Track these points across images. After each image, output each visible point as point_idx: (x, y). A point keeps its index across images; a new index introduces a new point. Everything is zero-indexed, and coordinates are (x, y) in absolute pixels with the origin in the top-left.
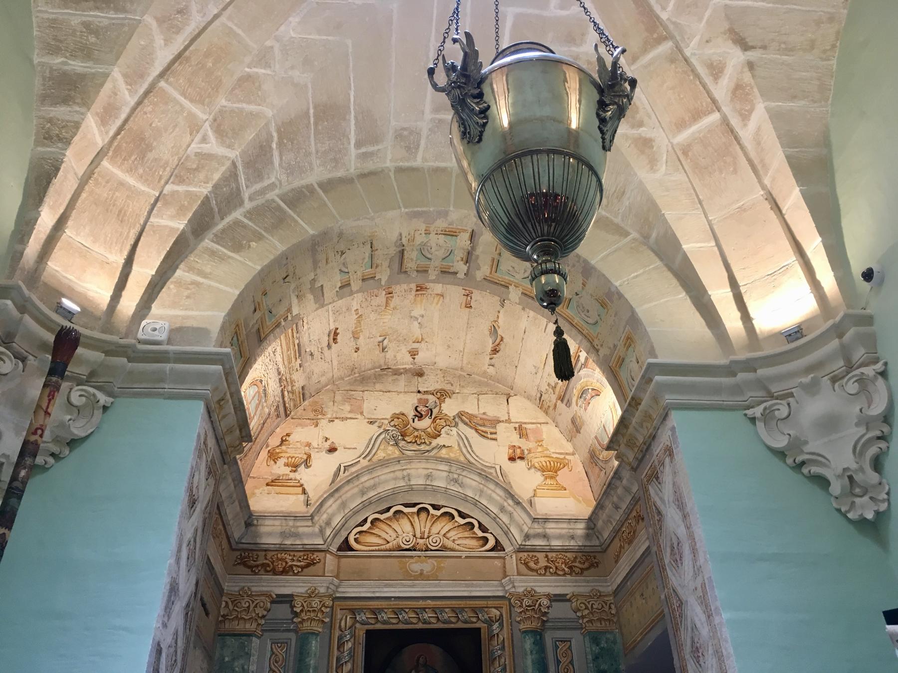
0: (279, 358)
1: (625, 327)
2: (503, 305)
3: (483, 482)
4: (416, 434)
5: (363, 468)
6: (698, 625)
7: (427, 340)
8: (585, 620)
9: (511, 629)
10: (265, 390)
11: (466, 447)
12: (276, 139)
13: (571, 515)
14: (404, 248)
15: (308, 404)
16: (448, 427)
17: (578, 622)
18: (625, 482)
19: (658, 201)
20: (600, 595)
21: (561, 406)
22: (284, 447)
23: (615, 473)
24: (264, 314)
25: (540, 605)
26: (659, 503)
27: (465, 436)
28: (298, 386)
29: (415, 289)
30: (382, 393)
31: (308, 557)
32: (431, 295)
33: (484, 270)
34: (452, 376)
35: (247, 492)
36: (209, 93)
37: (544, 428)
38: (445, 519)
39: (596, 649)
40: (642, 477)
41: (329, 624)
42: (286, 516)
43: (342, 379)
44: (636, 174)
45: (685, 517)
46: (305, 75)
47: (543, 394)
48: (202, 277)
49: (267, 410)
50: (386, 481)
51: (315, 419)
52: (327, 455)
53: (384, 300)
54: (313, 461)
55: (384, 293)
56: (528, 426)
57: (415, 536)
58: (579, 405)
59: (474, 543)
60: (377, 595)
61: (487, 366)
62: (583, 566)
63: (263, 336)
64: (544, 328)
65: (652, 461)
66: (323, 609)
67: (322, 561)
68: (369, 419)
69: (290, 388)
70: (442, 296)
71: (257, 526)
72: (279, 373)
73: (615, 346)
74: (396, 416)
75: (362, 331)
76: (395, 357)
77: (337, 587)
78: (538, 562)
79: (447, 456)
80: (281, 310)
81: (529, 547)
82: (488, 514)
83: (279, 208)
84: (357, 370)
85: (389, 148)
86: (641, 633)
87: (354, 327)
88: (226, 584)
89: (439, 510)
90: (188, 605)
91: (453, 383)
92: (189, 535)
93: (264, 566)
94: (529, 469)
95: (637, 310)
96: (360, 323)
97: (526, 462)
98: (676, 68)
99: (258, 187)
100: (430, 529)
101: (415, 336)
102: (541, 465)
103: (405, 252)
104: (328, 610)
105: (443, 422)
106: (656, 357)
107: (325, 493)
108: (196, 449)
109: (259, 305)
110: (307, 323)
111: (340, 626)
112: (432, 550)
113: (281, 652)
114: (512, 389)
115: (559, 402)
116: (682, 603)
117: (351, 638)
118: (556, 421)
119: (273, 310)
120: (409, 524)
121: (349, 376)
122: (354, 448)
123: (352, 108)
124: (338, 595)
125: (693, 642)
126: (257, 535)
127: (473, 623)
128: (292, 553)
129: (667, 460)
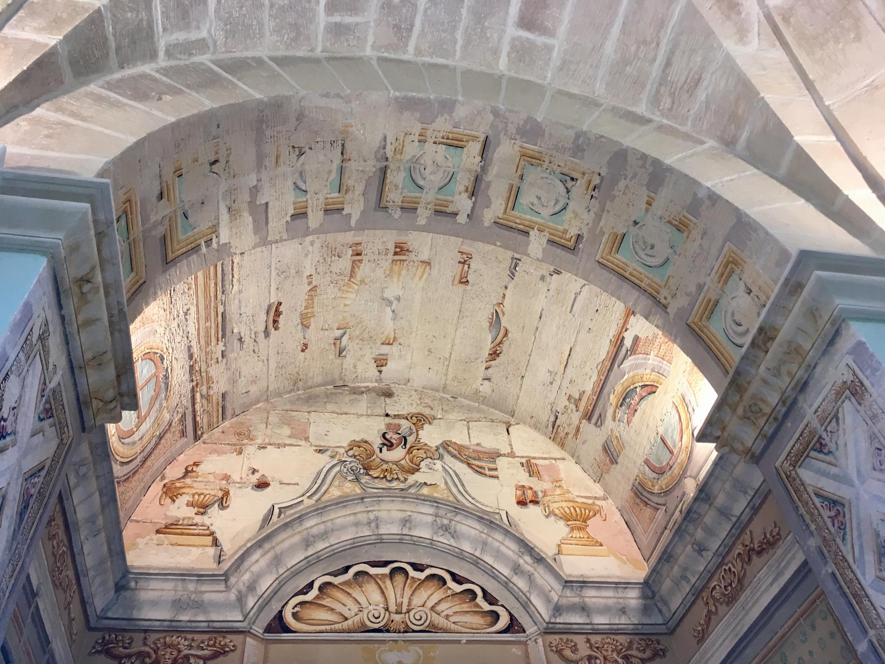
0: (192, 329)
3: (485, 531)
4: (385, 467)
7: (401, 340)
10: (166, 377)
11: (456, 486)
13: (618, 577)
14: (387, 163)
15: (229, 425)
16: (429, 460)
19: (754, 81)
22: (188, 481)
27: (455, 472)
29: (392, 250)
30: (336, 415)
31: (215, 642)
32: (414, 262)
33: (495, 209)
34: (431, 399)
35: (125, 541)
37: (561, 465)
38: (432, 585)
40: (778, 464)
42: (183, 575)
44: (720, 46)
47: (559, 415)
49: (167, 416)
50: (343, 528)
53: (349, 265)
55: (350, 252)
56: (540, 462)
57: (387, 609)
58: (617, 419)
59: (477, 620)
61: (480, 381)
63: (171, 256)
68: (316, 446)
69: (204, 392)
70: (429, 264)
72: (191, 356)
73: (700, 287)
74: (354, 444)
76: (355, 367)
78: (577, 650)
81: (561, 626)
82: (495, 577)
83: (211, 70)
84: (301, 383)
87: (304, 305)
89: (422, 571)
94: (547, 517)
100: (410, 599)
101: (386, 334)
102: (562, 511)
103: (389, 171)
105: (422, 453)
107: (249, 540)
110: (239, 281)
112: (414, 631)
114: (513, 416)
118: (576, 455)
119: (189, 213)
121: (290, 392)
122: (294, 484)
126: (133, 604)
128: (189, 636)
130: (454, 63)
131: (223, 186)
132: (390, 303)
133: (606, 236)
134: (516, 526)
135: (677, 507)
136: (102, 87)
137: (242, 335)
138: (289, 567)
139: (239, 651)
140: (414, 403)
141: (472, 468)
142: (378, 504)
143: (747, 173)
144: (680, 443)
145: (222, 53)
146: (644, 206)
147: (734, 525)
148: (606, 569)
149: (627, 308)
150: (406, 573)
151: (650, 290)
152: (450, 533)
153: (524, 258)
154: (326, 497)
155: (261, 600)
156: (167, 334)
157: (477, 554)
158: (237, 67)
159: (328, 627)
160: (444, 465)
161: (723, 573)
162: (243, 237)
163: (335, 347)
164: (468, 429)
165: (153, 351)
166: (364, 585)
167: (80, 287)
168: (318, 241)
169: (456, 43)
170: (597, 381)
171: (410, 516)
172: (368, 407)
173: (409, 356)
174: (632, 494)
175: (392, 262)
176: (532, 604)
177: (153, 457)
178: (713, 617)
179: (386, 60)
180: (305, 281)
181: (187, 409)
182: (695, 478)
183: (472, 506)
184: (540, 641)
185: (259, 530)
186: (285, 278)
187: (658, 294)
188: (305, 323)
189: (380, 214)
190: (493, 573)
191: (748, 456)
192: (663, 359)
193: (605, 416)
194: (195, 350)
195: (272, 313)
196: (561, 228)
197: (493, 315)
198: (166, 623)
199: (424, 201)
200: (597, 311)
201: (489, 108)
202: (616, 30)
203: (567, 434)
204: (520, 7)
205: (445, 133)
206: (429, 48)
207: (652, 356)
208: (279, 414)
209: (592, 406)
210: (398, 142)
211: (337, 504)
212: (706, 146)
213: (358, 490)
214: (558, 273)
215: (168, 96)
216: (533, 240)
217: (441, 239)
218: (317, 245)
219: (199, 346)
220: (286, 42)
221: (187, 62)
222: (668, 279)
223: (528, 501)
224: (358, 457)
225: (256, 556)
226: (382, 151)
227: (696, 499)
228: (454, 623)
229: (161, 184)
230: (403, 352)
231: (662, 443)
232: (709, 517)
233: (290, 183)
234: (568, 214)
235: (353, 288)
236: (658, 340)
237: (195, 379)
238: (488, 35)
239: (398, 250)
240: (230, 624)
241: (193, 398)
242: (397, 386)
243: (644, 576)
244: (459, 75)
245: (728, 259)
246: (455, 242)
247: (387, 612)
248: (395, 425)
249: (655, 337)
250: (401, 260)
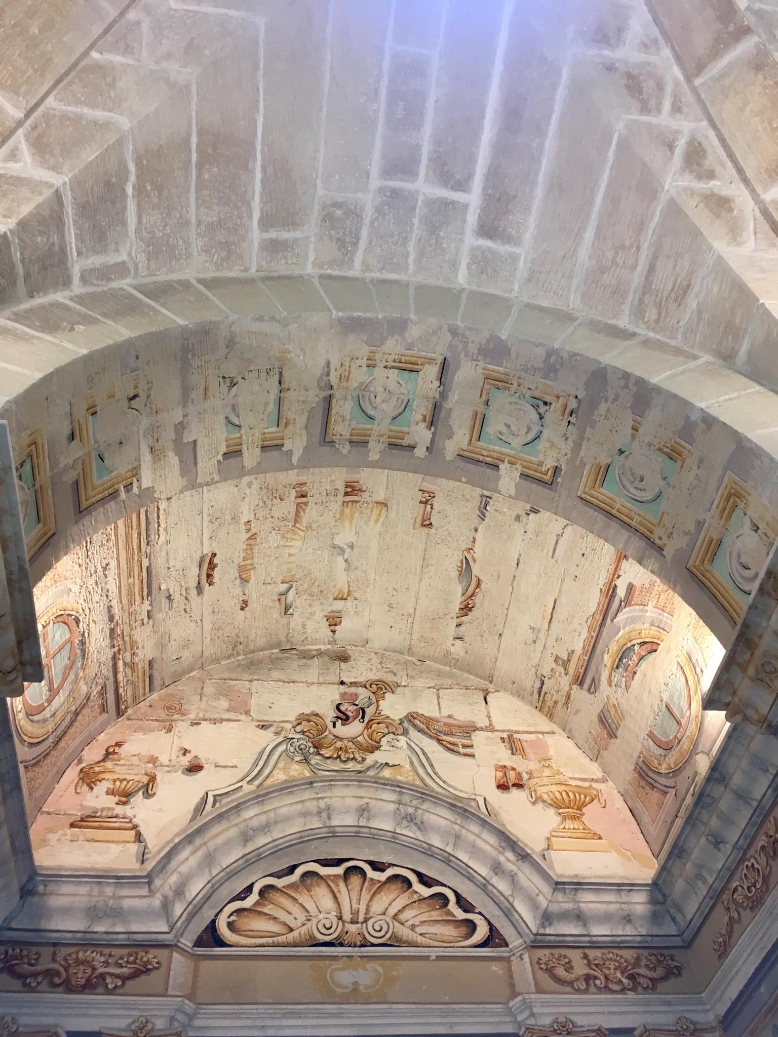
0: (112, 586)
3: (459, 822)
4: (339, 744)
7: (356, 595)
10: (83, 643)
12: (132, 178)
13: (621, 877)
15: (157, 698)
16: (392, 736)
22: (109, 764)
24: (89, 453)
27: (422, 749)
28: (146, 652)
30: (281, 683)
31: (136, 958)
32: (367, 503)
34: (394, 663)
36: (29, 77)
37: (549, 739)
38: (395, 888)
42: (99, 877)
43: (216, 660)
44: (710, 248)
46: (189, 70)
47: (546, 680)
49: (84, 689)
50: (287, 819)
51: (168, 721)
52: (184, 776)
54: (160, 786)
55: (293, 493)
57: (340, 918)
58: (613, 684)
59: (449, 932)
61: (450, 641)
63: (84, 504)
64: (552, 550)
68: (258, 721)
70: (385, 505)
72: (111, 618)
73: (700, 524)
74: (303, 718)
76: (304, 626)
77: (191, 1017)
78: (572, 968)
80: (120, 465)
81: (552, 938)
82: (470, 879)
83: (130, 296)
84: (241, 647)
85: (313, 239)
87: (242, 556)
89: (383, 870)
91: (395, 671)
93: (49, 974)
94: (534, 803)
97: (527, 791)
98: (765, 78)
99: (97, 261)
100: (368, 905)
101: (339, 586)
102: (552, 796)
103: (334, 401)
105: (382, 728)
107: (178, 834)
110: (166, 530)
112: (373, 945)
114: (491, 682)
121: (229, 657)
122: (232, 767)
123: (259, 147)
128: (106, 951)
130: (406, 279)
131: (145, 422)
132: (343, 551)
133: (588, 467)
134: (495, 816)
135: (688, 790)
136: (9, 319)
137: (171, 592)
138: (224, 866)
139: (163, 970)
140: (374, 668)
141: (443, 744)
142: (330, 789)
143: (748, 391)
144: (688, 712)
145: (144, 277)
146: (629, 431)
147: (755, 811)
148: (606, 867)
149: (617, 551)
150: (363, 872)
151: (642, 529)
152: (416, 824)
153: (495, 496)
154: (269, 782)
155: (191, 907)
156: (83, 592)
157: (449, 849)
158: (159, 292)
159: (270, 940)
160: (409, 741)
161: (745, 871)
162: (168, 480)
163: (280, 604)
164: (438, 698)
165: (67, 612)
166: (313, 889)
168: (257, 482)
169: (408, 256)
170: (587, 638)
171: (367, 804)
172: (319, 674)
173: (366, 614)
174: (636, 775)
175: (343, 504)
176: (517, 912)
177: (67, 737)
178: (736, 926)
179: (330, 277)
180: (243, 527)
181: (108, 680)
182: (708, 754)
183: (443, 792)
184: (526, 957)
185: (190, 822)
186: (220, 525)
187: (652, 533)
188: (243, 576)
189: (326, 450)
190: (468, 872)
191: (765, 725)
192: (662, 610)
193: (599, 681)
194: (117, 611)
196: (534, 459)
197: (462, 563)
198: (79, 935)
199: (376, 434)
200: (583, 555)
201: (446, 327)
202: (589, 234)
203: (556, 702)
204: (479, 214)
205: (396, 357)
206: (378, 263)
207: (650, 608)
208: (216, 683)
209: (583, 668)
210: (343, 367)
211: (281, 790)
212: (700, 362)
213: (307, 774)
214: (536, 512)
215: (81, 326)
216: (503, 475)
217: (398, 476)
218: (256, 485)
219: (120, 606)
220: (216, 262)
221: (105, 289)
222: (662, 517)
223: (510, 784)
224: (307, 733)
226: (325, 378)
227: (709, 779)
228: (421, 934)
229: (72, 423)
230: (360, 609)
231: (668, 712)
232: (726, 802)
233: (221, 418)
234: (542, 445)
235: (299, 535)
236: (656, 588)
237: (116, 645)
238: (445, 246)
239: (349, 490)
240: (153, 936)
241: (115, 666)
242: (354, 648)
243: (652, 876)
244: (412, 291)
245: (730, 491)
246: (415, 479)
247: (341, 922)
248: (351, 694)
249: (653, 584)
250: (353, 502)
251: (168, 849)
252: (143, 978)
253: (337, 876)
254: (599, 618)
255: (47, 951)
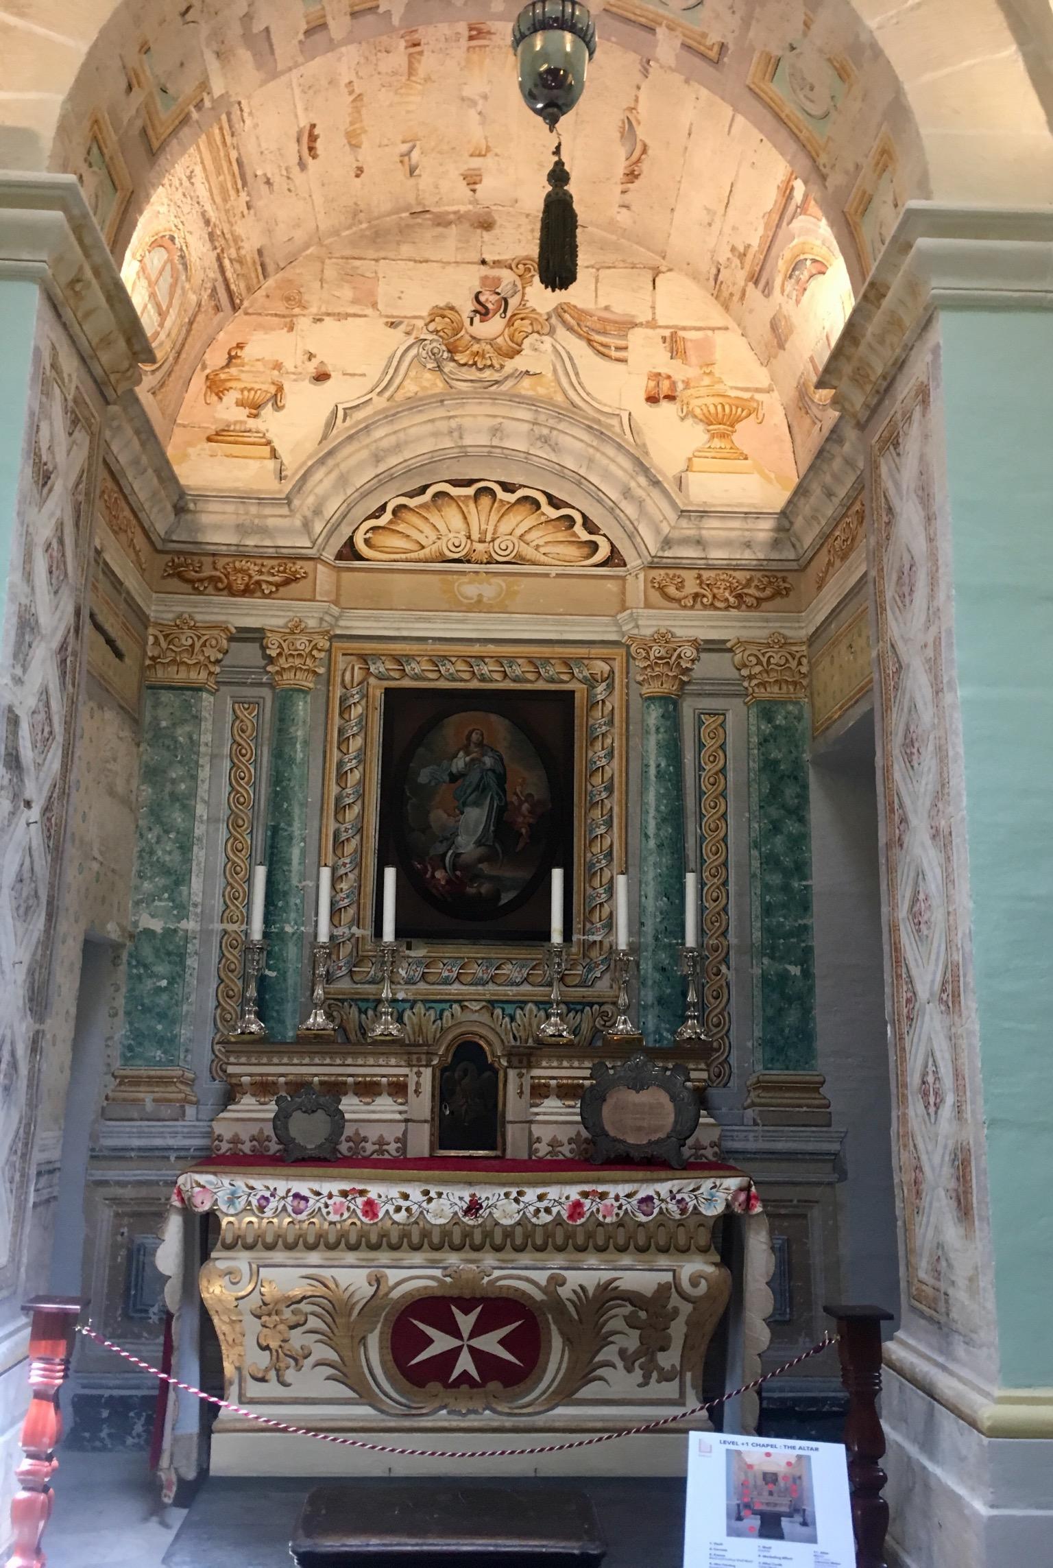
0: (202, 191)
1: (880, 125)
2: (647, 71)
3: (595, 444)
4: (476, 348)
5: (376, 413)
6: (920, 705)
7: (497, 150)
8: (754, 682)
9: (627, 694)
10: (182, 257)
13: (749, 505)
16: (536, 335)
17: (741, 685)
18: (847, 447)
20: (785, 643)
21: (753, 293)
22: (233, 371)
23: (833, 431)
24: (151, 95)
25: (679, 657)
26: (892, 492)
27: (568, 353)
28: (248, 250)
29: (466, 34)
32: (499, 47)
37: (719, 337)
38: (525, 509)
39: (766, 728)
41: (325, 677)
42: (243, 498)
43: (336, 233)
45: (929, 519)
48: (12, 13)
49: (193, 298)
50: (418, 439)
55: (402, 44)
59: (572, 552)
60: (405, 633)
62: (761, 595)
63: (156, 144)
65: (892, 413)
66: (315, 652)
67: (311, 576)
69: (234, 255)
71: (195, 512)
74: (438, 313)
75: (365, 132)
76: (437, 187)
77: (337, 619)
78: (683, 587)
79: (530, 393)
80: (185, 87)
81: (669, 561)
82: (599, 501)
86: (841, 708)
88: (153, 608)
89: (513, 492)
90: (63, 647)
92: (45, 532)
95: (907, 87)
96: (359, 112)
102: (705, 411)
104: (322, 655)
105: (526, 326)
106: (928, 196)
107: (309, 458)
108: (33, 379)
109: (137, 76)
110: (251, 114)
111: (343, 680)
113: (248, 717)
114: (664, 258)
115: (751, 285)
116: (901, 667)
117: (361, 699)
119: (168, 85)
120: (459, 517)
121: (349, 227)
124: (338, 632)
125: (908, 729)
126: (197, 528)
127: (563, 682)
128: (259, 561)
129: (917, 415)
137: (269, 175)
146: (801, 26)
157: (582, 472)
167: (73, 289)
172: (457, 249)
177: (187, 347)
180: (345, 91)
184: (641, 576)
195: (305, 139)
225: (319, 474)
239: (474, 33)
248: (494, 278)
250: (480, 47)
251: (302, 472)
252: (293, 585)
253: (467, 497)
254: (776, 217)
255: (208, 560)
